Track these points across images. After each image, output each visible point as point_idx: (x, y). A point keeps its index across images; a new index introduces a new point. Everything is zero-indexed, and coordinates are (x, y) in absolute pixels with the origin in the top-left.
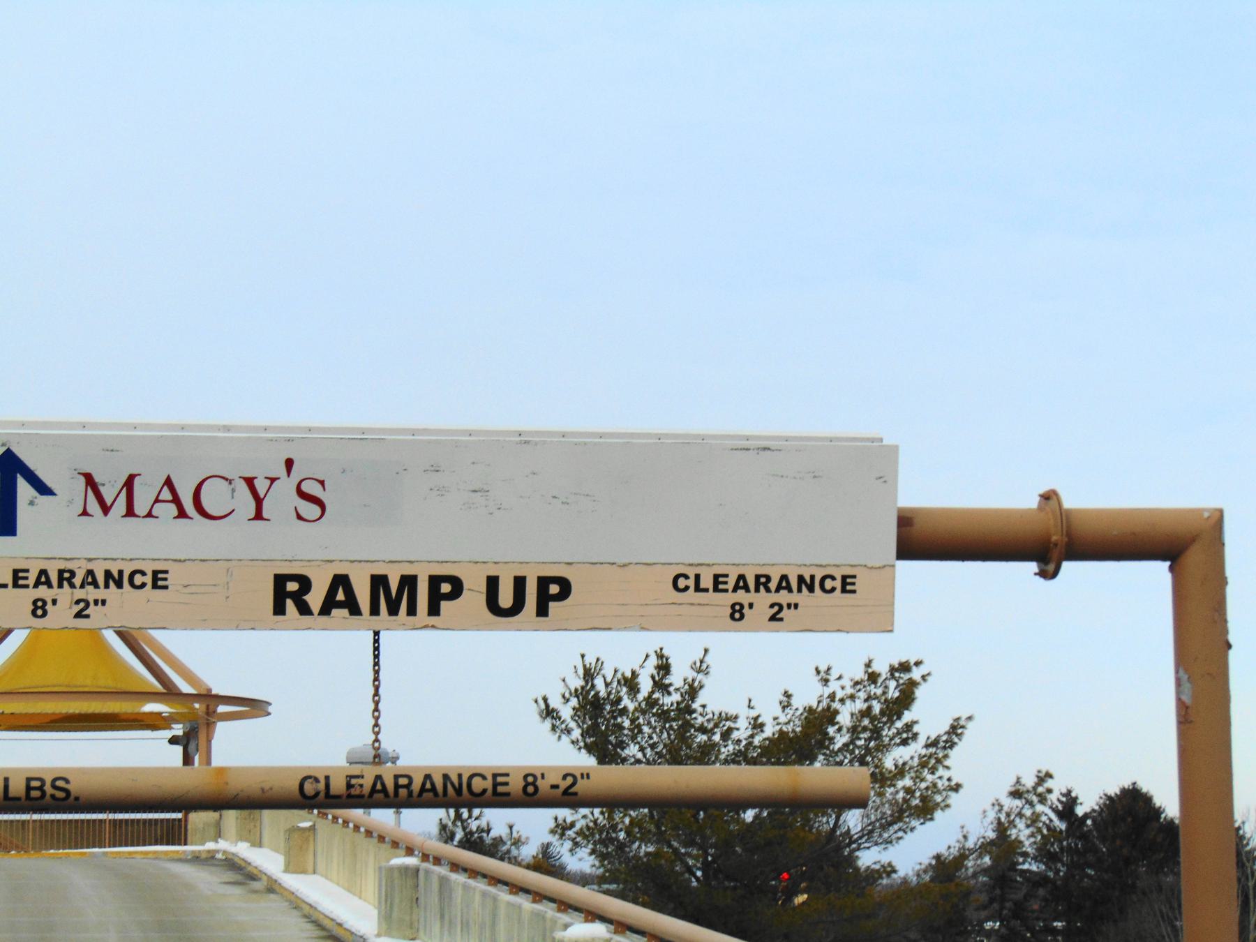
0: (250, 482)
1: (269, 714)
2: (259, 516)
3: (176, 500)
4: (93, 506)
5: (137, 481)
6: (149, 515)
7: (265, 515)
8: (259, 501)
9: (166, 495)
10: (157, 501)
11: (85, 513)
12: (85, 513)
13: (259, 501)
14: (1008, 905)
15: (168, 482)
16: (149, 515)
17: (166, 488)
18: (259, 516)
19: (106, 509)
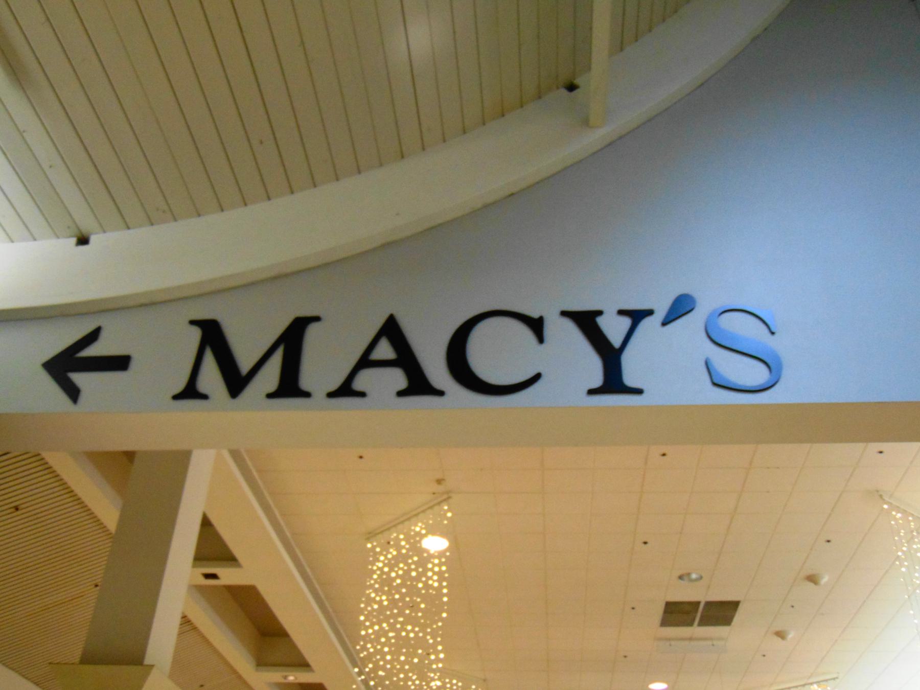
0: (587, 321)
1: (152, 666)
2: (613, 383)
3: (406, 359)
4: (211, 377)
5: (312, 333)
6: (346, 390)
7: (630, 378)
8: (611, 357)
9: (385, 351)
10: (365, 362)
11: (191, 392)
12: (191, 392)
13: (611, 357)
14: (369, 608)
15: (391, 329)
16: (346, 390)
17: (616, 341)
18: (613, 383)
19: (236, 383)
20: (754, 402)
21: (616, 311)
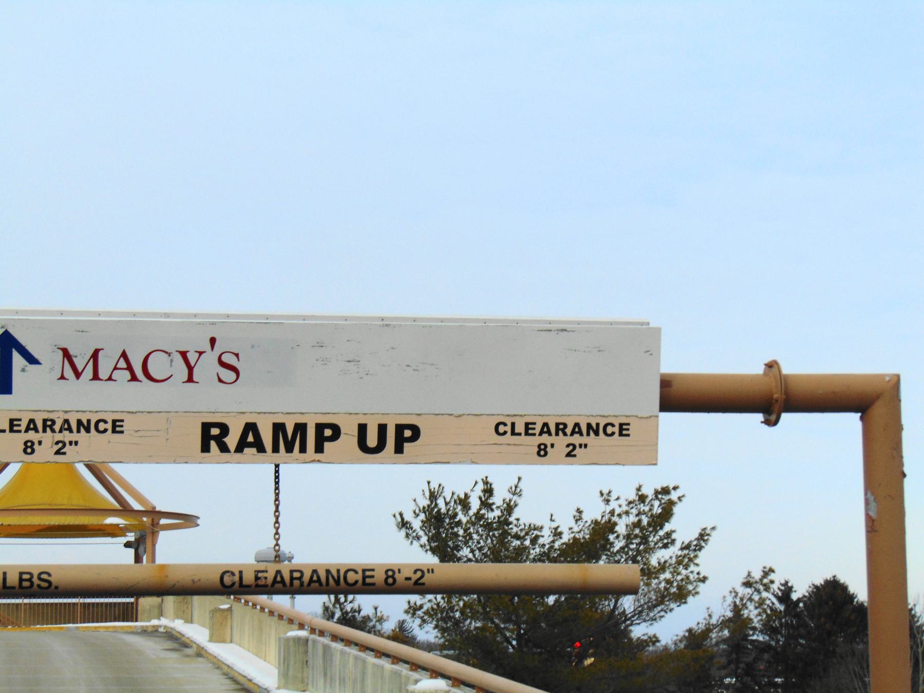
0: (184, 354)
1: (198, 525)
2: (190, 379)
3: (130, 368)
4: (69, 372)
5: (101, 354)
6: (110, 379)
7: (195, 379)
8: (190, 369)
9: (122, 364)
10: (115, 368)
11: (62, 377)
12: (62, 377)
13: (190, 369)
14: (742, 665)
15: (124, 355)
16: (110, 379)
17: (122, 359)
18: (190, 379)
19: (78, 375)
20: (394, 438)
21: (681, 486)
